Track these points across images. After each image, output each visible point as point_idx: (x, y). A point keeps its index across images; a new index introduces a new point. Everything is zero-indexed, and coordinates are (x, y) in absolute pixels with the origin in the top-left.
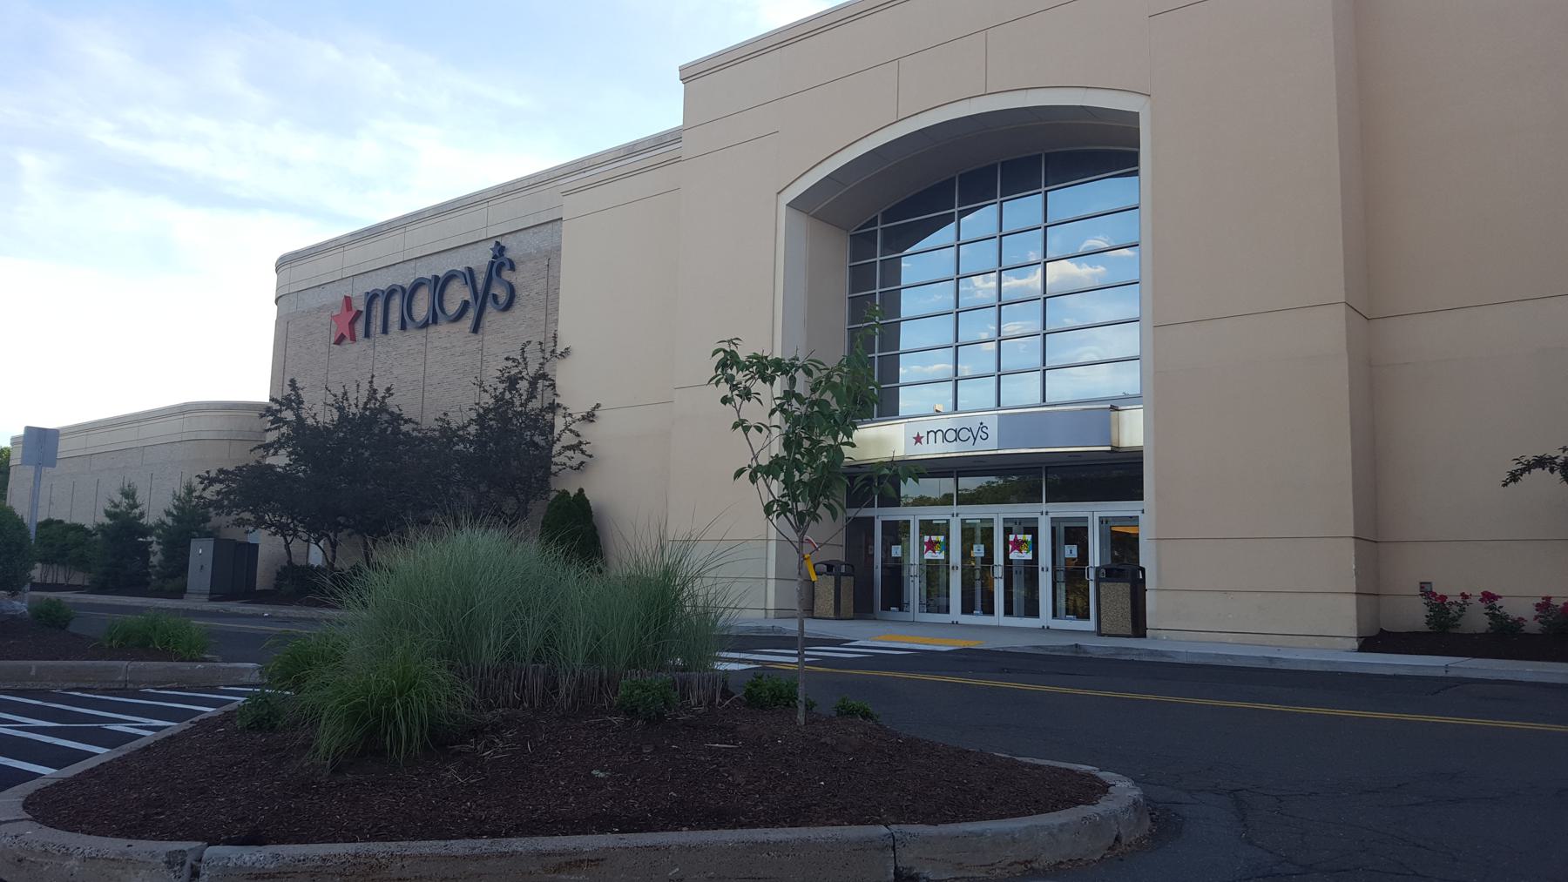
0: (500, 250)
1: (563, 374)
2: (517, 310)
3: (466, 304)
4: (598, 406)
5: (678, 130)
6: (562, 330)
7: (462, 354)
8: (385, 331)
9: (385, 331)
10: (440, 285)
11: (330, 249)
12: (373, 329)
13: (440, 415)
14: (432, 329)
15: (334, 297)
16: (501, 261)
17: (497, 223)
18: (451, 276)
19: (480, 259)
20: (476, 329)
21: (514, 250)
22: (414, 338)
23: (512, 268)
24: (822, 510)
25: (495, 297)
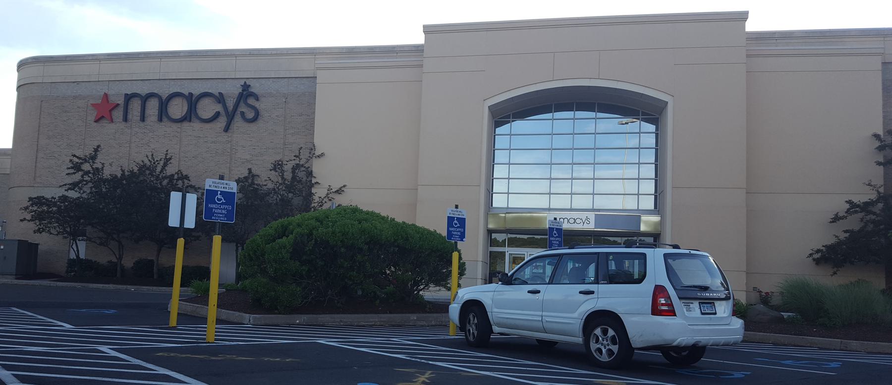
0: (246, 87)
1: (318, 167)
2: (260, 123)
3: (217, 115)
4: (344, 186)
5: (422, 46)
6: (317, 141)
7: (214, 142)
8: (143, 118)
9: (143, 118)
10: (193, 101)
11: (87, 60)
12: (130, 116)
13: (449, 211)
14: (186, 124)
15: (101, 91)
16: (246, 93)
17: (246, 71)
18: (205, 95)
19: (232, 90)
20: (226, 129)
21: (256, 88)
22: (167, 128)
23: (257, 98)
24: (77, 177)
25: (243, 114)
